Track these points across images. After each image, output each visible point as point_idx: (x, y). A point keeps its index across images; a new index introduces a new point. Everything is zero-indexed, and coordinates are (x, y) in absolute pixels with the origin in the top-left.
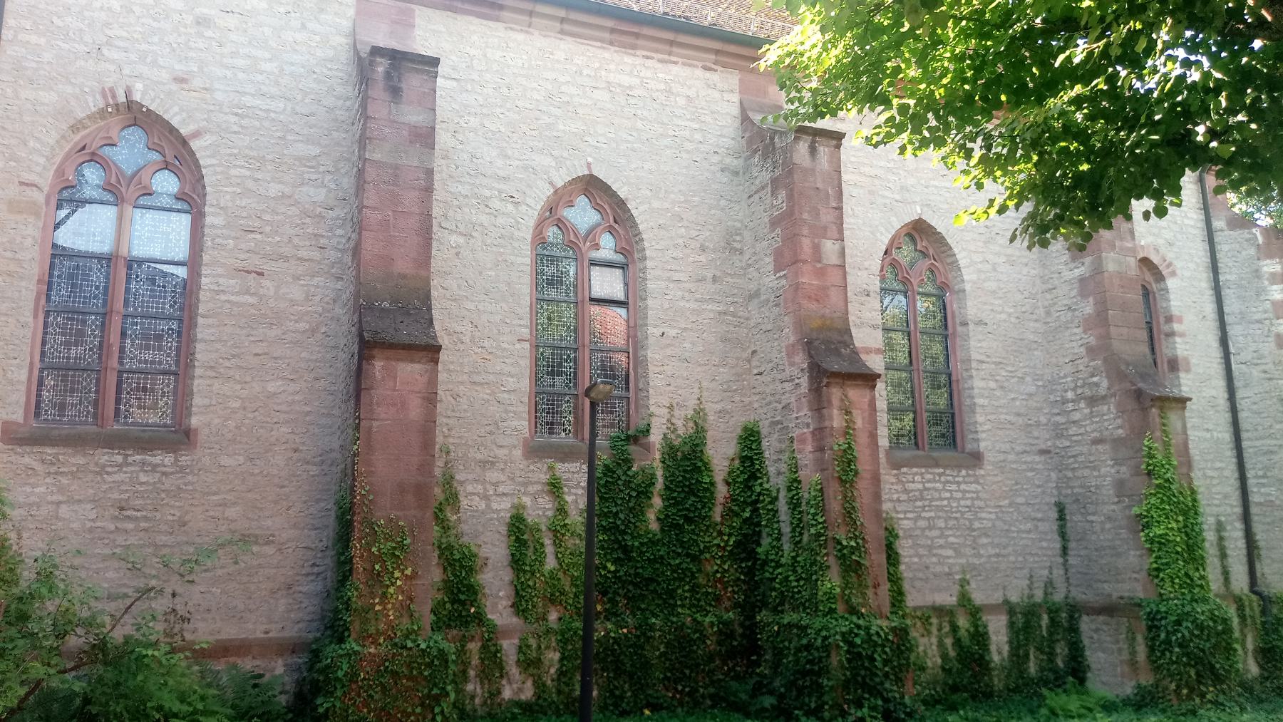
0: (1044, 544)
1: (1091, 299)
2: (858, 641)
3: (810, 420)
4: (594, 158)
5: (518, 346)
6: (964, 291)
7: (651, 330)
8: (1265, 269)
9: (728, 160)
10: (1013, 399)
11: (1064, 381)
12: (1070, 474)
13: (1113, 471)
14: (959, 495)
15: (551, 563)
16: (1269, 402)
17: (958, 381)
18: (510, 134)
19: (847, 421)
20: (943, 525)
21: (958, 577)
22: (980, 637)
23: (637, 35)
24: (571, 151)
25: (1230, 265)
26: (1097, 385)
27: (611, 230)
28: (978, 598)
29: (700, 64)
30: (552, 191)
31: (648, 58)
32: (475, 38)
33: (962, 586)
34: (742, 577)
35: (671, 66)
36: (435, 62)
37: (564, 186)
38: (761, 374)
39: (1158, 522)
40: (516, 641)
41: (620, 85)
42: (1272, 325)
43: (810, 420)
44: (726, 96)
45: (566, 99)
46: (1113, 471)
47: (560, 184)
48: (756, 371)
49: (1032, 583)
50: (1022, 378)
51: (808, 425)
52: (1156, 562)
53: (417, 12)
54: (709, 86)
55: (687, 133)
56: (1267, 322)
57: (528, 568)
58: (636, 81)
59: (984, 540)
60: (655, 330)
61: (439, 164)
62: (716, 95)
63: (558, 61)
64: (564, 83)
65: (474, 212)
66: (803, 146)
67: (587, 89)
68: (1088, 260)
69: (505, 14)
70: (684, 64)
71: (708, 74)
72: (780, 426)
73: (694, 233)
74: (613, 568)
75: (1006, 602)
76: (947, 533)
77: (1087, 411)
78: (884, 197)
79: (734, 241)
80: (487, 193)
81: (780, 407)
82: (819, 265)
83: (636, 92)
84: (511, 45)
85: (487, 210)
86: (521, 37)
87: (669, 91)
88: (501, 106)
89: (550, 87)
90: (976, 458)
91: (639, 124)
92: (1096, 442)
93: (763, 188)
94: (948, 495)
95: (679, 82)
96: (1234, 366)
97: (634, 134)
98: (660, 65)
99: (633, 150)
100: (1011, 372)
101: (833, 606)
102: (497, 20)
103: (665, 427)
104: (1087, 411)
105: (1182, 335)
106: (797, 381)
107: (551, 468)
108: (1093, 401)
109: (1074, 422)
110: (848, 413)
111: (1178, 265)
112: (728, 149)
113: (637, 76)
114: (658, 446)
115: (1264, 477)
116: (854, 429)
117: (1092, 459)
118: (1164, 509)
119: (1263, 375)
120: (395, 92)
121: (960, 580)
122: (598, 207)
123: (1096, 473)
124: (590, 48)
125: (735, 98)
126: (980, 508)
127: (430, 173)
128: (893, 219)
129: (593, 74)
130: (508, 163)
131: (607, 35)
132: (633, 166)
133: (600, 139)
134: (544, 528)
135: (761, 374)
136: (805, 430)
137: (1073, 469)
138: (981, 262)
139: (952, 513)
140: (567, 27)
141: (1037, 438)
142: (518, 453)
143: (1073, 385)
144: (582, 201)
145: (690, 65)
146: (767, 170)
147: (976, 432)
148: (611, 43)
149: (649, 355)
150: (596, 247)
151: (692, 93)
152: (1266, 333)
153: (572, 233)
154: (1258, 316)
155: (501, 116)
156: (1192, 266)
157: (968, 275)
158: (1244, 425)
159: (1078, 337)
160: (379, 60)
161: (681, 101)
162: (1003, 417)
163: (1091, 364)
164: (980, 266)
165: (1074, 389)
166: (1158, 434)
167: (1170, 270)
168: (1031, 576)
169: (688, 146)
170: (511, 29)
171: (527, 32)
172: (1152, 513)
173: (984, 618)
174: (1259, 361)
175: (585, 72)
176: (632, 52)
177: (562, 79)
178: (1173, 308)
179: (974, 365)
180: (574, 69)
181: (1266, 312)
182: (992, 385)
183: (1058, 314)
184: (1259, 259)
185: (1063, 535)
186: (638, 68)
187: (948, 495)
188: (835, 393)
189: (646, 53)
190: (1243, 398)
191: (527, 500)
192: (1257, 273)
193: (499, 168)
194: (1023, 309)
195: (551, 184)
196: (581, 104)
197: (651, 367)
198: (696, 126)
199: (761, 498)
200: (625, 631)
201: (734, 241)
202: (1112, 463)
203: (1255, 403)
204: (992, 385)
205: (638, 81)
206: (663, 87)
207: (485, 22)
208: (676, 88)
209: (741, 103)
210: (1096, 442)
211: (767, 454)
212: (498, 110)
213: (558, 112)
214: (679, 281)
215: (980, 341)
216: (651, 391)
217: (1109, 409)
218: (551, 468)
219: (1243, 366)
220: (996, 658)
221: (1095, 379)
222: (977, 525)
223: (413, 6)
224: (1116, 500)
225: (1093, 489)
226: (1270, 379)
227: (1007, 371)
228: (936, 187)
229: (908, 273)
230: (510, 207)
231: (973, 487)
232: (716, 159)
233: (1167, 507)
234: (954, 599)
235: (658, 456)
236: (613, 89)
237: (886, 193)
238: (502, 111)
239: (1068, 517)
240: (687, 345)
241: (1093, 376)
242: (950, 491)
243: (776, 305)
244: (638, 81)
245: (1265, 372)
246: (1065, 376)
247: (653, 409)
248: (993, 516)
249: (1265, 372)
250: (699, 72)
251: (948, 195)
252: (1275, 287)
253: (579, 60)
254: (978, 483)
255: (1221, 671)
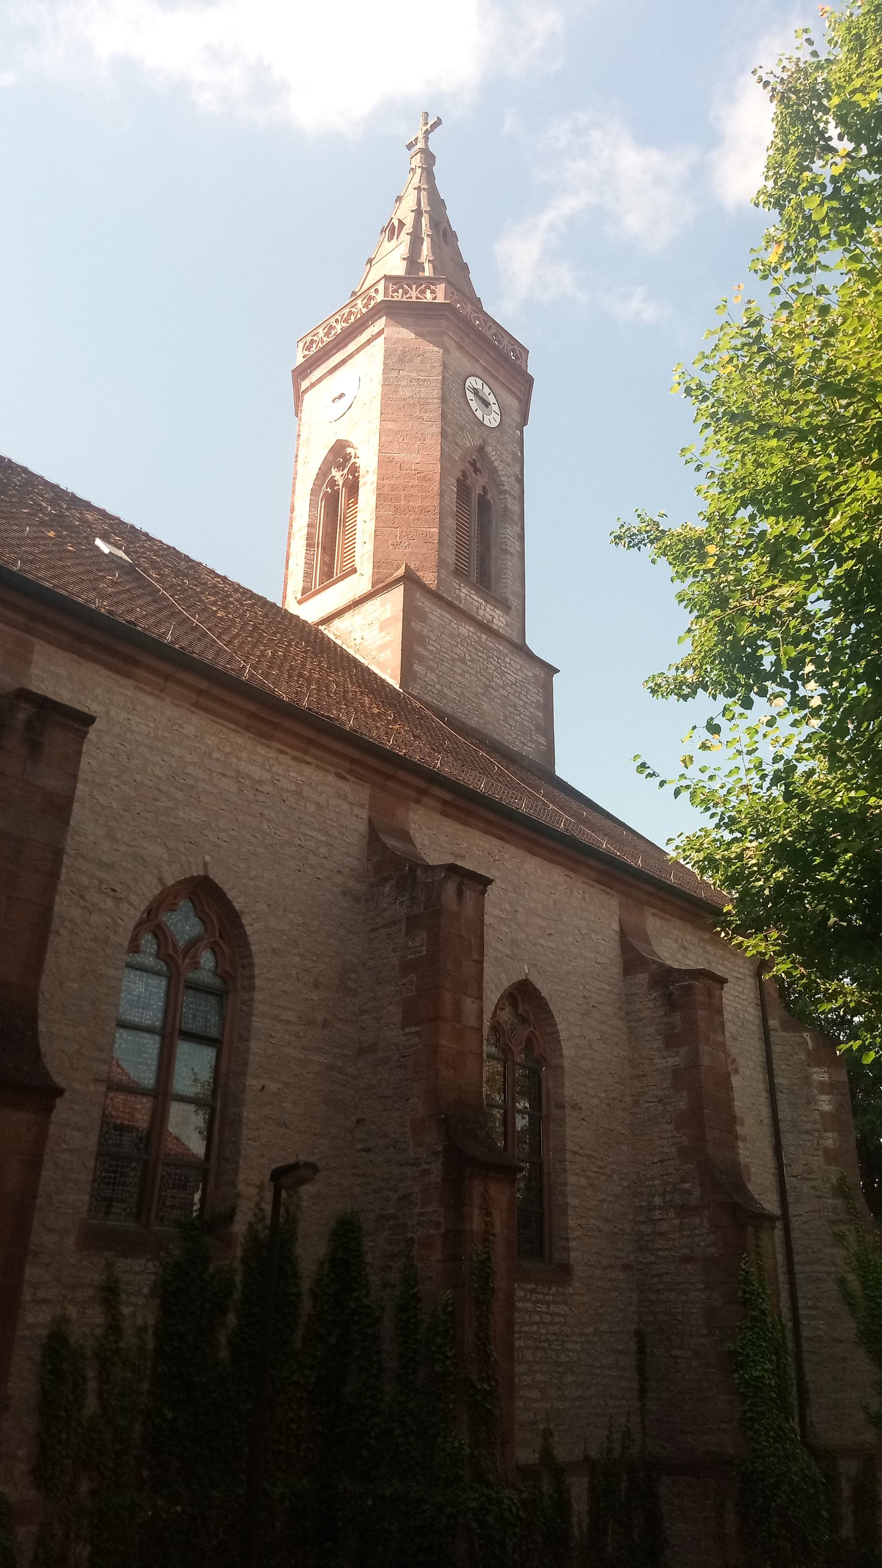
0: (624, 1384)
1: (685, 1094)
2: (491, 1519)
3: (441, 1219)
4: (212, 857)
5: (92, 1088)
6: (562, 1068)
7: (251, 1081)
8: (815, 1077)
9: (351, 883)
10: (601, 1200)
11: (651, 1183)
12: (653, 1297)
13: (703, 1296)
14: (548, 1319)
15: (91, 1405)
16: (818, 1223)
17: (549, 1174)
18: (121, 812)
19: (486, 1225)
20: (530, 1358)
21: (541, 1427)
22: (562, 1505)
23: (275, 726)
24: (188, 845)
25: (783, 1067)
26: (688, 1192)
27: (214, 949)
28: (561, 1454)
29: (333, 770)
30: (160, 889)
31: (282, 752)
32: (99, 691)
33: (546, 1439)
34: (320, 1429)
35: (304, 767)
36: (89, 720)
37: (173, 886)
38: (367, 1150)
39: (754, 1361)
40: (35, 1528)
41: (250, 777)
42: (821, 1137)
43: (441, 1219)
44: (356, 810)
45: (190, 782)
46: (703, 1296)
47: (170, 882)
48: (359, 1146)
49: (611, 1433)
50: (610, 1176)
51: (438, 1225)
52: (750, 1410)
53: (37, 648)
54: (339, 796)
55: (313, 845)
56: (816, 1134)
57: (62, 1414)
58: (267, 776)
59: (569, 1379)
60: (254, 1082)
61: (70, 844)
62: (346, 807)
63: (188, 737)
64: (191, 763)
65: (65, 902)
66: (451, 888)
67: (215, 774)
68: (683, 1050)
69: (139, 672)
70: (317, 767)
71: (340, 783)
72: (392, 1222)
73: (309, 964)
74: (170, 1415)
75: (587, 1458)
76: (535, 1368)
77: (676, 1222)
78: (497, 950)
79: (349, 979)
80: (85, 881)
81: (395, 1196)
82: (459, 1026)
83: (267, 788)
84: (139, 708)
85: (82, 903)
86: (150, 701)
87: (299, 794)
88: (116, 777)
89: (175, 765)
90: (565, 1271)
91: (265, 826)
92: (685, 1260)
93: (394, 923)
94: (537, 1318)
95: (310, 785)
96: (787, 1179)
97: (258, 836)
98: (292, 763)
99: (255, 854)
100: (602, 1168)
101: (461, 1472)
102: (127, 675)
103: (251, 1213)
104: (676, 1222)
105: (744, 1139)
106: (426, 1166)
107: (109, 1265)
108: (683, 1210)
109: (661, 1234)
110: (488, 1213)
111: (741, 1061)
112: (352, 870)
113: (269, 771)
114: (241, 1240)
115: (814, 1307)
116: (494, 1234)
117: (680, 1280)
118: (761, 1346)
119: (813, 1192)
120: (34, 747)
121: (544, 1429)
122: (204, 919)
123: (683, 1298)
124: (223, 729)
125: (364, 814)
126: (567, 1336)
127: (59, 853)
128: (503, 976)
129: (223, 758)
130: (115, 847)
131: (243, 719)
132: (252, 874)
133: (222, 835)
134: (89, 1353)
135: (367, 1150)
136: (433, 1231)
137: (657, 1291)
138: (579, 1037)
139: (541, 1341)
140: (203, 700)
141: (622, 1250)
142: (70, 1240)
143: (662, 1189)
144: (185, 905)
145: (324, 769)
146: (402, 904)
147: (567, 1239)
148: (247, 728)
149: (245, 1114)
150: (196, 965)
151: (322, 800)
152: (815, 1146)
153: (171, 945)
154: (808, 1126)
155: (115, 789)
156: (751, 1064)
157: (568, 1050)
158: (796, 1247)
159: (670, 1135)
160: (24, 705)
161: (311, 808)
162: (592, 1221)
163: (684, 1167)
164: (577, 1040)
165: (663, 1195)
166: (753, 1256)
167: (734, 1067)
168: (611, 1425)
169: (313, 859)
170: (141, 689)
171: (158, 697)
172: (748, 1350)
173: (568, 1482)
174: (809, 1176)
175: (215, 755)
176: (267, 742)
177: (189, 758)
178: (736, 1109)
179: (568, 1156)
180: (203, 749)
181: (815, 1123)
182: (584, 1182)
183: (647, 1105)
184: (809, 1065)
185: (641, 1370)
186: (271, 762)
187: (537, 1318)
188: (477, 1187)
189: (279, 746)
190: (794, 1216)
191: (72, 1311)
192: (807, 1080)
193: (103, 852)
194: (614, 1096)
195: (161, 880)
196: (205, 791)
197: (246, 1132)
198: (323, 838)
199: (356, 1318)
200: (179, 1508)
201: (349, 979)
202: (702, 1287)
203: (805, 1223)
204: (584, 1182)
205: (269, 776)
206: (293, 787)
207: (113, 675)
208: (307, 791)
209: (370, 820)
210: (685, 1260)
211: (369, 1258)
212: (113, 781)
213: (179, 795)
214: (287, 1022)
215: (574, 1128)
216: (242, 1163)
217: (701, 1222)
218: (109, 1265)
219: (795, 1179)
220: (576, 1533)
221: (687, 1186)
222: (563, 1358)
223: (33, 639)
224: (706, 1332)
225: (679, 1317)
226: (820, 1197)
227: (598, 1167)
228: (543, 946)
229: (510, 1040)
230: (110, 903)
231: (563, 1309)
232: (339, 879)
233: (764, 1344)
234: (537, 1456)
235: (239, 1253)
236: (242, 780)
237: (499, 946)
238: (118, 783)
239: (648, 1351)
240: (288, 1105)
241: (684, 1181)
242: (540, 1313)
243: (401, 1067)
244: (269, 776)
245: (814, 1188)
246: (653, 1178)
247: (241, 1187)
248: (577, 1347)
249: (814, 1188)
250: (331, 779)
251: (552, 957)
252: (823, 1097)
253: (210, 740)
254: (566, 1304)
255: (813, 1546)
